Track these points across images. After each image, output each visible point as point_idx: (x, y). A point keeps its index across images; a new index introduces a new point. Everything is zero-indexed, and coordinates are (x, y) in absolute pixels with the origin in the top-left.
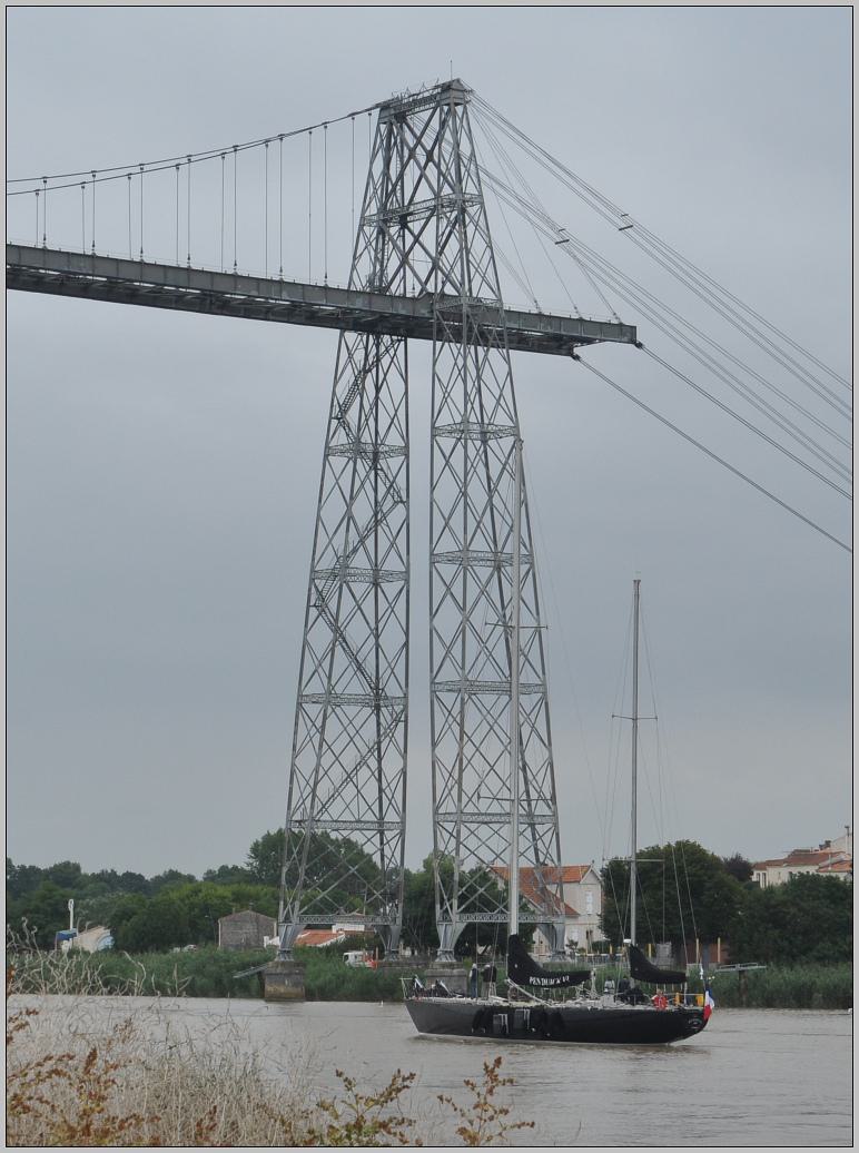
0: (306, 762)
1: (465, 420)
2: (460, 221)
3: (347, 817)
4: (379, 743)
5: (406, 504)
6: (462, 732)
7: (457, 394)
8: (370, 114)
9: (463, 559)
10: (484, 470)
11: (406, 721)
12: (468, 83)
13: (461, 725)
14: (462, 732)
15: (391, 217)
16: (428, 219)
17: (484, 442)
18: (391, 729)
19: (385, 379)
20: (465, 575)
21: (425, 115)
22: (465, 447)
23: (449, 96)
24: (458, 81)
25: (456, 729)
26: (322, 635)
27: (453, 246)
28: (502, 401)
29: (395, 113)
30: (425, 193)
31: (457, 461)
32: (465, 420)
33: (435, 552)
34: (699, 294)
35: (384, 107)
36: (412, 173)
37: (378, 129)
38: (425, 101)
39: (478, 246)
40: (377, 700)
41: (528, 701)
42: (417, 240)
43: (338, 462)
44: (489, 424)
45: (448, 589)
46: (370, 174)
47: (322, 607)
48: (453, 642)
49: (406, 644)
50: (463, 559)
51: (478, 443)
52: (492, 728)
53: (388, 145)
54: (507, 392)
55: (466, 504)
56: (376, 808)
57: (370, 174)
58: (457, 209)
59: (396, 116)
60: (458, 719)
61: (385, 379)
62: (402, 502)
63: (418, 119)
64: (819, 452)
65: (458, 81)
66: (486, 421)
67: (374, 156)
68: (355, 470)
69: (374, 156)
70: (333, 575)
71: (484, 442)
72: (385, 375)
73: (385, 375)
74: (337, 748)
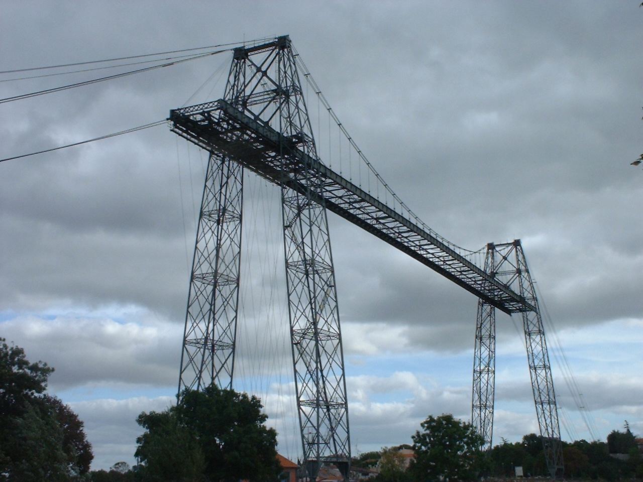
37: (233, 61)
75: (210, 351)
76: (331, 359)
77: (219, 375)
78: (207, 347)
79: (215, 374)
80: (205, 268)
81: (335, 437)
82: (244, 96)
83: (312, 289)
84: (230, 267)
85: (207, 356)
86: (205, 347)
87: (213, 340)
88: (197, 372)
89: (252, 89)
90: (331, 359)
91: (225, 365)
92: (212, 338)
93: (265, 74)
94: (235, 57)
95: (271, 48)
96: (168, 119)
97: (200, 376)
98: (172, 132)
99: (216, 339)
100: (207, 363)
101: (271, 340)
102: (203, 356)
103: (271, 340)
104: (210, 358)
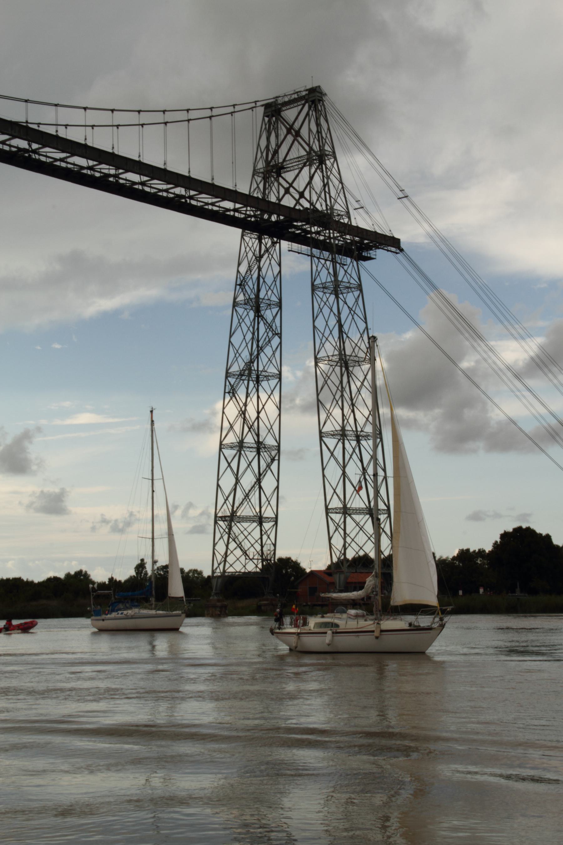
1: (343, 428)
5: (280, 335)
6: (345, 533)
8: (253, 110)
9: (342, 435)
10: (357, 417)
11: (279, 460)
13: (345, 530)
14: (345, 533)
16: (284, 160)
17: (358, 441)
19: (263, 408)
22: (343, 444)
24: (319, 87)
25: (342, 532)
31: (338, 453)
32: (343, 428)
34: (452, 263)
35: (267, 106)
37: (263, 119)
43: (240, 310)
44: (362, 431)
45: (332, 454)
48: (321, 192)
49: (277, 487)
50: (241, 445)
51: (354, 443)
59: (275, 111)
60: (328, 170)
61: (263, 408)
62: (277, 334)
63: (290, 114)
64: (503, 306)
65: (319, 87)
66: (359, 429)
68: (344, 448)
71: (358, 441)
72: (264, 406)
73: (264, 406)
75: (255, 382)
76: (357, 348)
77: (273, 393)
78: (251, 379)
79: (261, 407)
80: (350, 298)
81: (321, 174)
82: (310, 166)
83: (328, 195)
84: (323, 304)
85: (334, 306)
86: (258, 372)
87: (249, 381)
88: (241, 405)
89: (297, 179)
90: (357, 348)
91: (272, 397)
92: (256, 369)
93: (298, 134)
94: (266, 114)
95: (299, 103)
96: (26, 436)
97: (246, 409)
98: (291, 252)
99: (261, 368)
100: (251, 395)
101: (184, 653)
102: (247, 389)
103: (184, 653)
104: (255, 390)
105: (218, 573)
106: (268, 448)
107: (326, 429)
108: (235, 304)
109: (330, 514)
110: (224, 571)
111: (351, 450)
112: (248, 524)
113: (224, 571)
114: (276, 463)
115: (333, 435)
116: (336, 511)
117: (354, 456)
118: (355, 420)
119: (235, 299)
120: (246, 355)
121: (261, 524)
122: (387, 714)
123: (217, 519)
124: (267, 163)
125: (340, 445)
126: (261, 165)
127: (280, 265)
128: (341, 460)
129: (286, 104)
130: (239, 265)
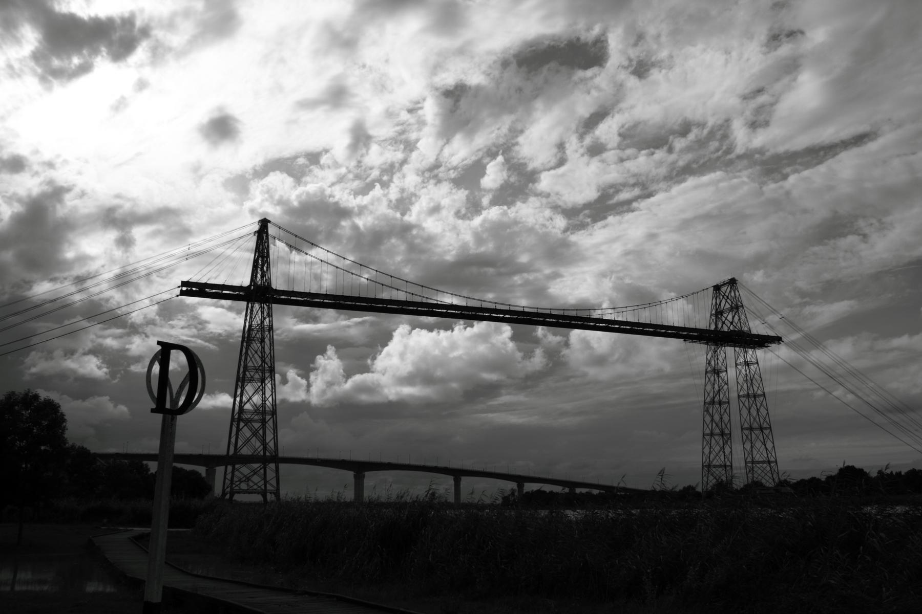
0: (707, 450)
2: (737, 311)
3: (717, 464)
4: (724, 446)
5: (728, 384)
7: (745, 387)
12: (736, 278)
14: (752, 457)
15: (718, 313)
16: (723, 309)
18: (727, 442)
20: (750, 422)
21: (725, 288)
23: (732, 282)
25: (751, 456)
26: (708, 419)
27: (736, 317)
28: (759, 388)
29: (717, 288)
30: (728, 306)
31: (747, 404)
32: (748, 394)
33: (744, 427)
36: (724, 301)
37: (713, 293)
38: (726, 284)
39: (743, 317)
40: (722, 434)
41: (767, 432)
42: (726, 319)
43: (709, 375)
46: (712, 303)
47: (707, 411)
50: (712, 434)
51: (753, 399)
52: (724, 294)
53: (715, 297)
54: (761, 385)
55: (750, 415)
56: (724, 462)
57: (712, 303)
58: (736, 307)
62: (726, 384)
63: (724, 289)
67: (713, 299)
68: (749, 402)
69: (713, 299)
70: (710, 403)
74: (713, 447)
82: (732, 312)
105: (704, 490)
106: (726, 434)
107: (738, 362)
108: (706, 372)
109: (744, 431)
110: (707, 490)
111: (752, 402)
112: (716, 464)
113: (707, 490)
114: (729, 441)
115: (743, 396)
116: (746, 429)
117: (754, 405)
118: (753, 390)
119: (706, 370)
120: (711, 395)
121: (726, 468)
122: (417, 497)
123: (703, 466)
124: (717, 310)
125: (747, 400)
126: (714, 312)
127: (725, 353)
128: (748, 407)
129: (722, 285)
130: (707, 355)
